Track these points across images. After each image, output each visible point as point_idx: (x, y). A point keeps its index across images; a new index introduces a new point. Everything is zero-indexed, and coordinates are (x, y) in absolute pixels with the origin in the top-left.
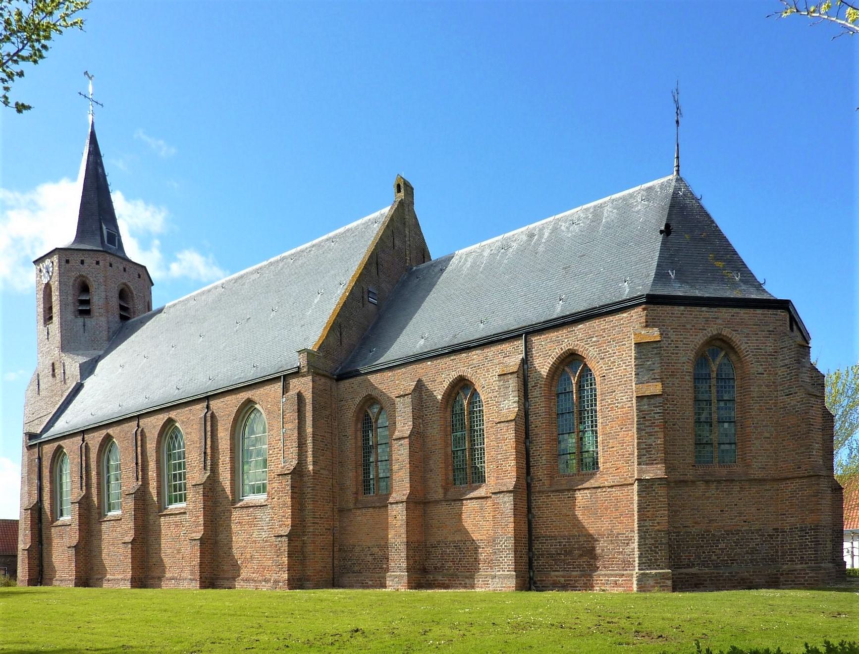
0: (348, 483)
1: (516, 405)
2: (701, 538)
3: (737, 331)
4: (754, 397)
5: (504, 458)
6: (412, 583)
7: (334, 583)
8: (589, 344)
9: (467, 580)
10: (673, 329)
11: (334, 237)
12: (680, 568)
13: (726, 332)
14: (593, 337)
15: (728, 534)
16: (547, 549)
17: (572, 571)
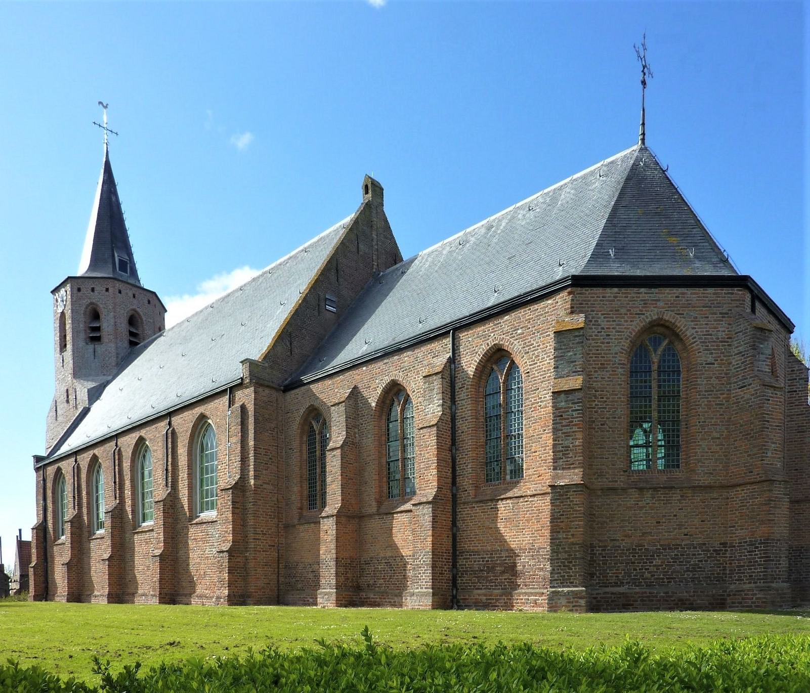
0: (293, 498)
1: (440, 409)
2: (632, 553)
3: (683, 314)
4: (702, 391)
5: (427, 467)
6: (342, 601)
7: (279, 600)
8: (514, 337)
9: (396, 598)
10: (605, 314)
11: (309, 247)
12: (606, 587)
14: (518, 329)
15: (665, 549)
16: (471, 565)
17: (494, 589)
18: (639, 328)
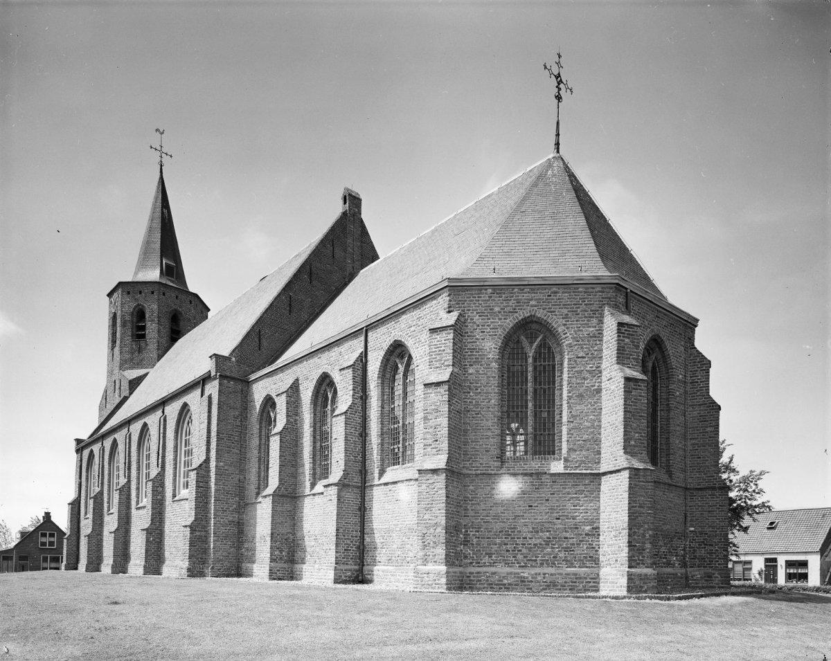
13: (540, 314)
18: (511, 325)
